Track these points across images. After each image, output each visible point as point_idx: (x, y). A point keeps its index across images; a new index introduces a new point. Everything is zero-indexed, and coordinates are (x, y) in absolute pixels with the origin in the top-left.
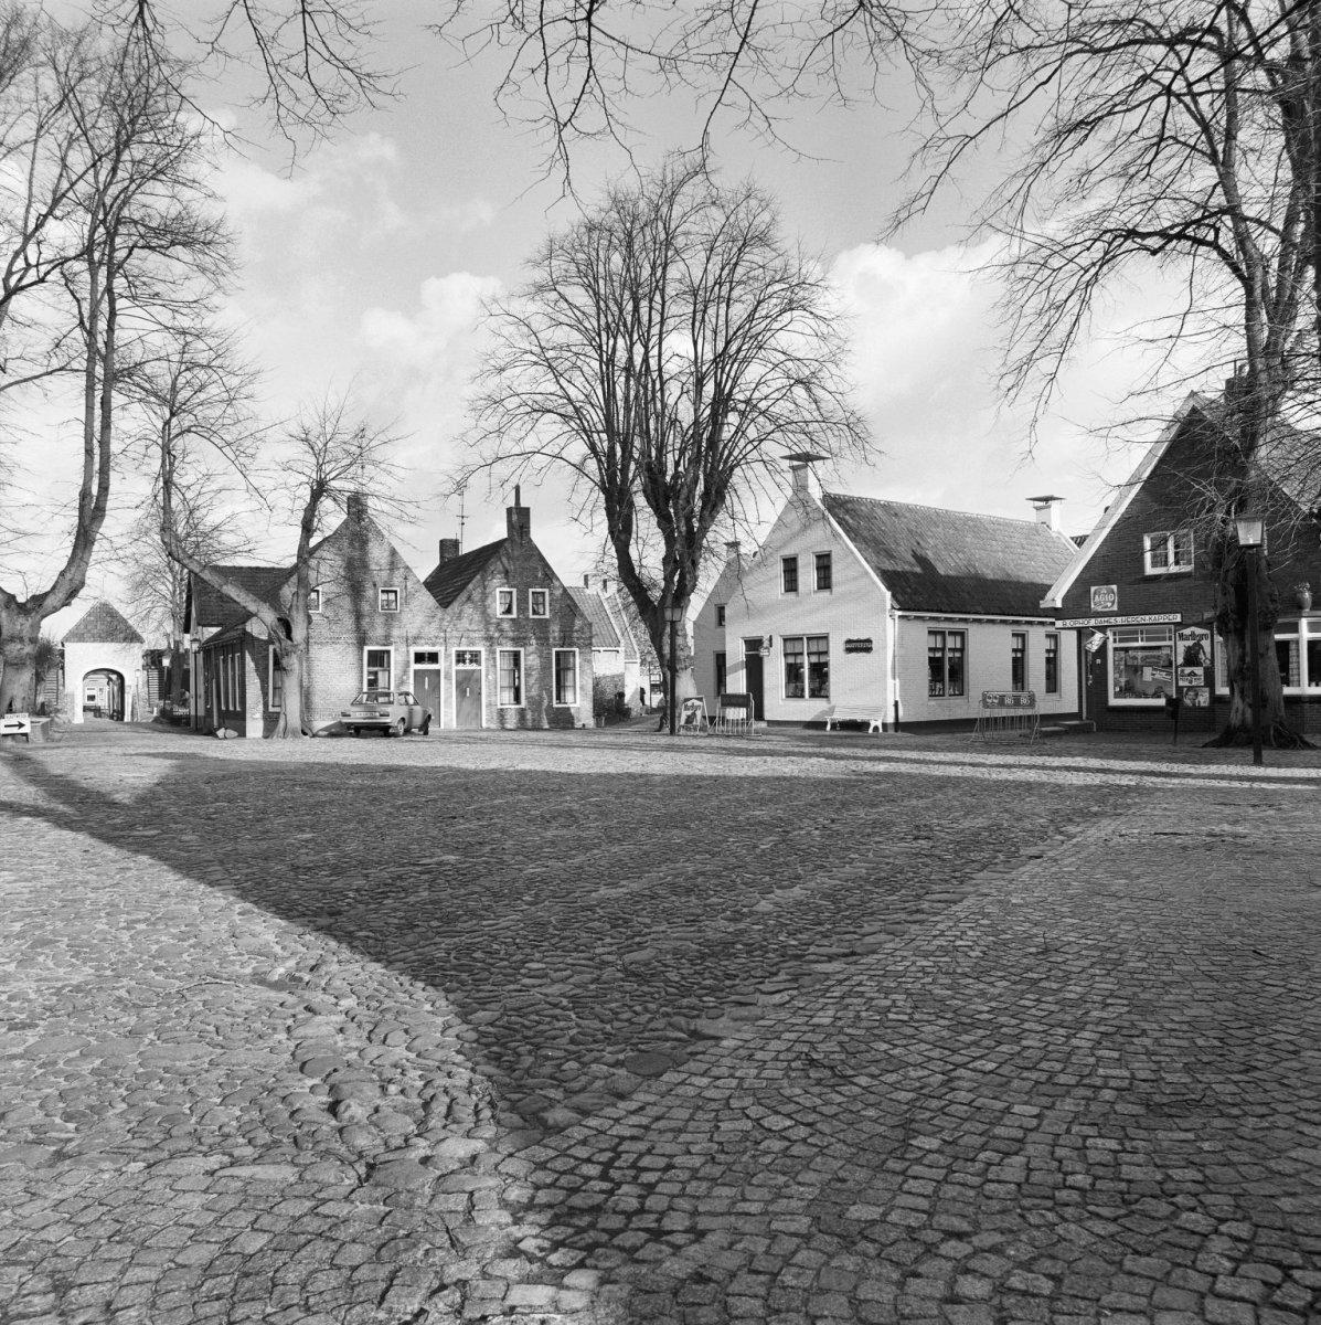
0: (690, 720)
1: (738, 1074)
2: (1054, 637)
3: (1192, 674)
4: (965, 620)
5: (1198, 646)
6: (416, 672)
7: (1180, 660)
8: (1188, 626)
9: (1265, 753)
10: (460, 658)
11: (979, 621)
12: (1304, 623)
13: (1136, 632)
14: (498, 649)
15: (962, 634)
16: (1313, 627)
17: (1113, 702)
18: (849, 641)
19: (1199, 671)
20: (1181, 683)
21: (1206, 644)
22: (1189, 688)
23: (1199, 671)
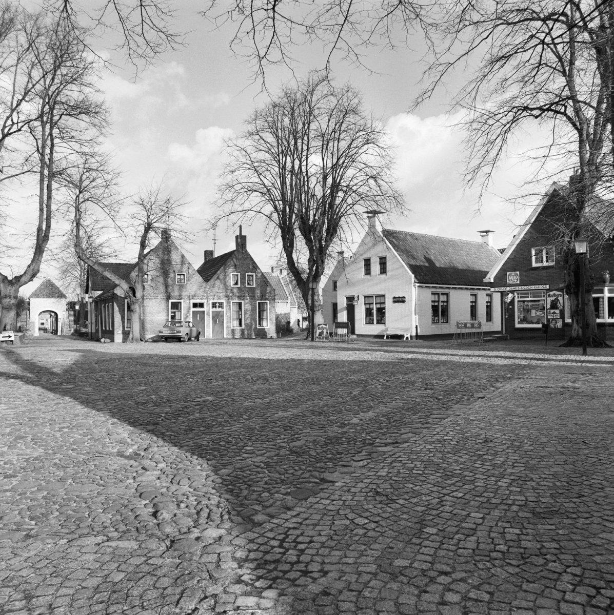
0: (321, 334)
1: (343, 498)
2: (490, 296)
3: (554, 313)
4: (449, 288)
5: (557, 300)
6: (193, 312)
7: (549, 306)
8: (552, 291)
9: (588, 350)
10: (214, 305)
11: (455, 288)
12: (606, 289)
13: (528, 293)
14: (232, 301)
15: (447, 294)
16: (610, 291)
17: (517, 326)
18: (395, 298)
19: (557, 311)
20: (549, 317)
21: (560, 299)
22: (553, 319)
23: (557, 311)
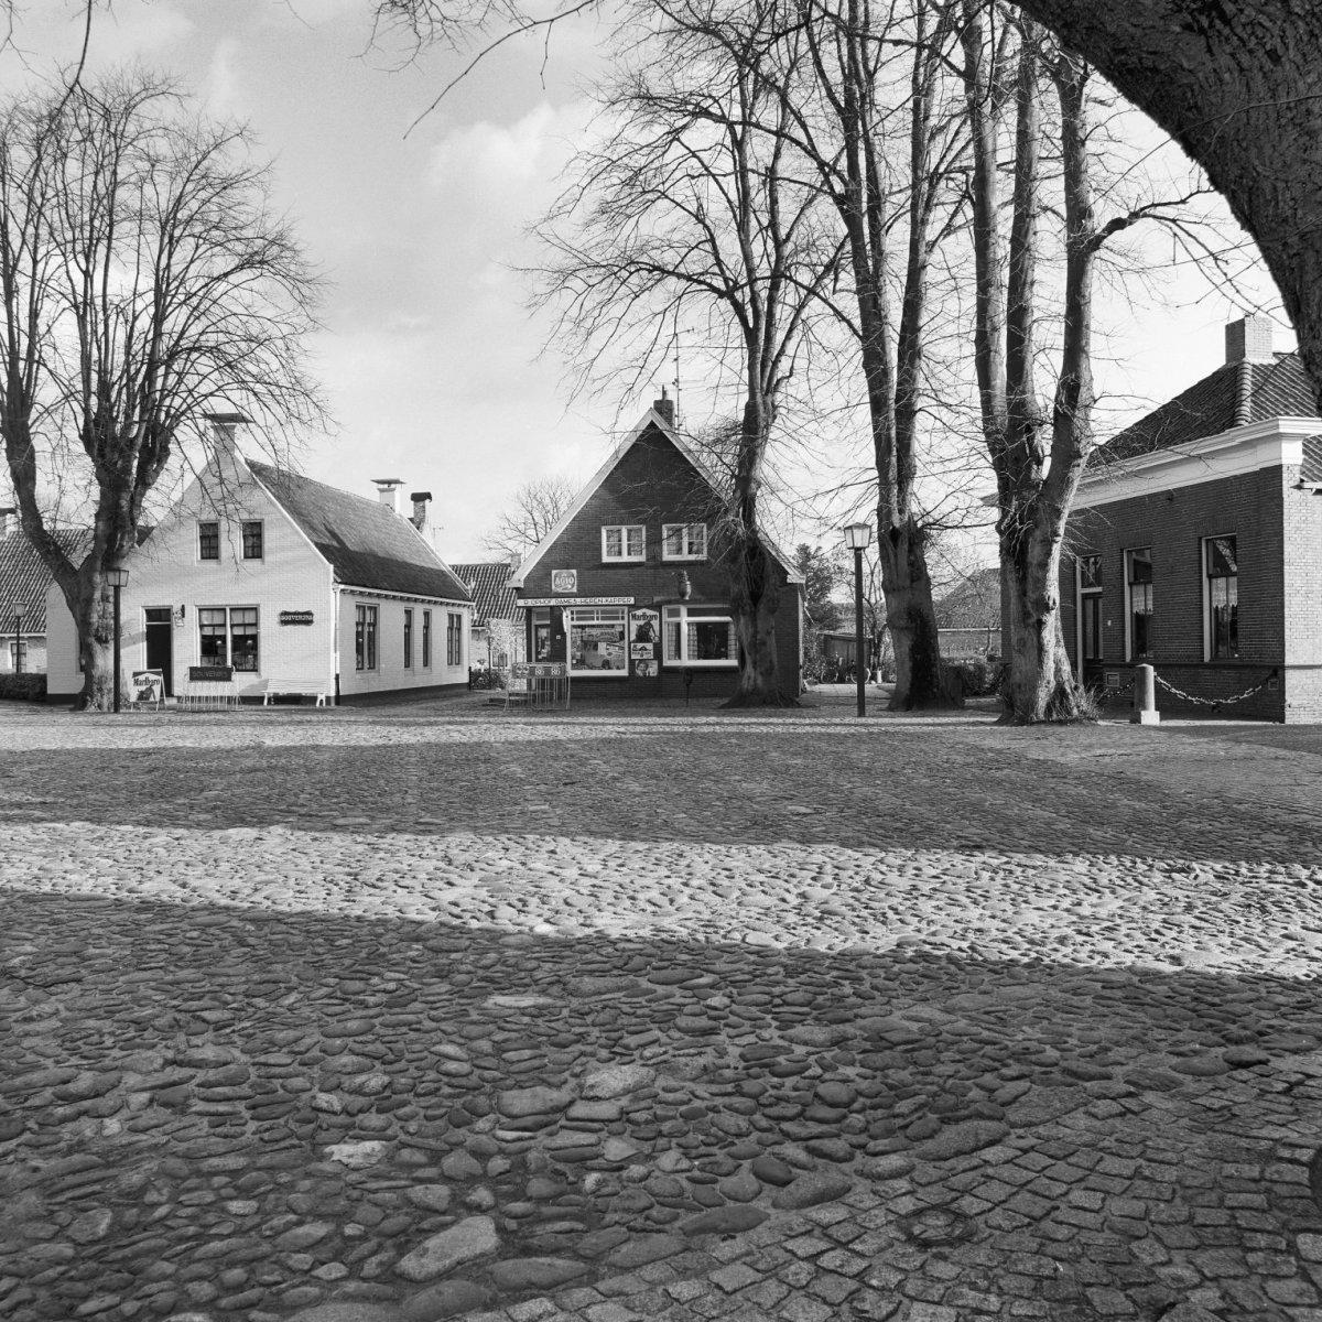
4: (378, 596)
7: (633, 637)
11: (386, 597)
15: (374, 609)
19: (650, 646)
21: (655, 623)
23: (650, 646)
